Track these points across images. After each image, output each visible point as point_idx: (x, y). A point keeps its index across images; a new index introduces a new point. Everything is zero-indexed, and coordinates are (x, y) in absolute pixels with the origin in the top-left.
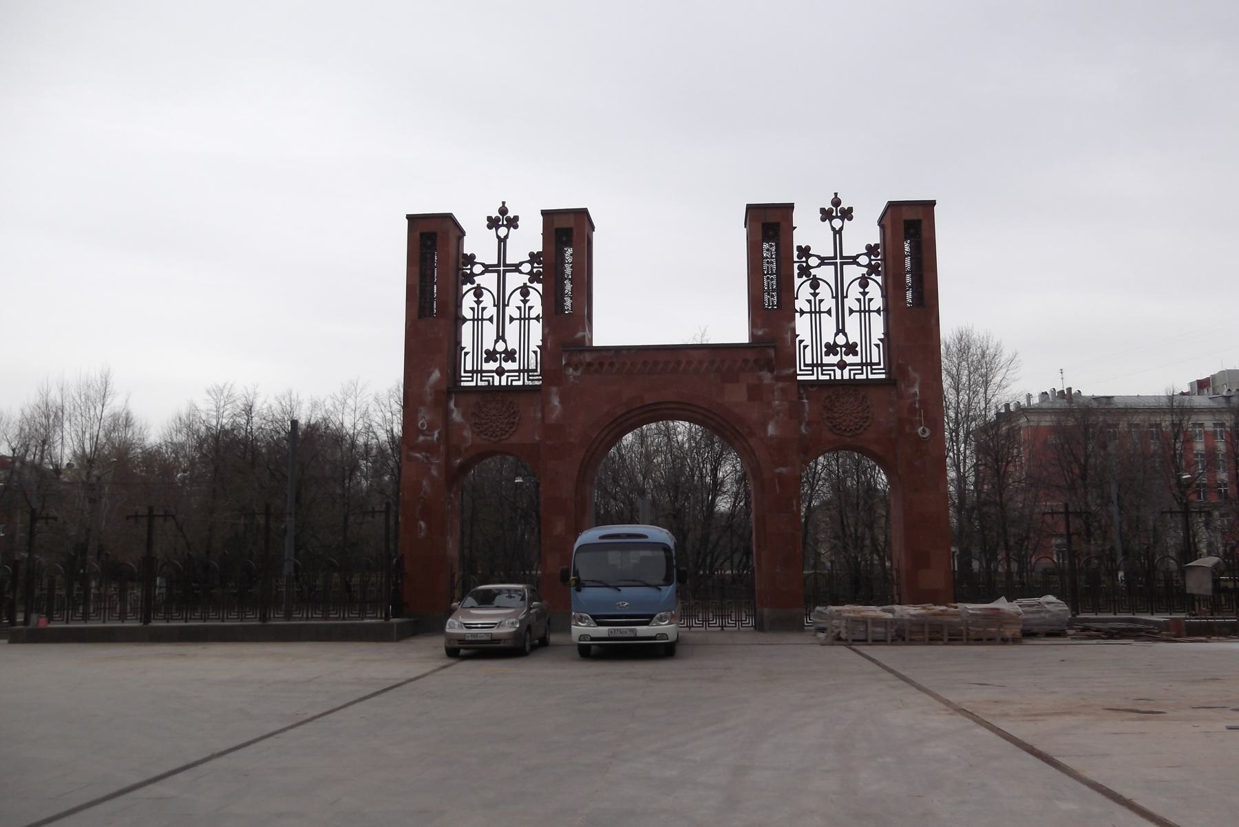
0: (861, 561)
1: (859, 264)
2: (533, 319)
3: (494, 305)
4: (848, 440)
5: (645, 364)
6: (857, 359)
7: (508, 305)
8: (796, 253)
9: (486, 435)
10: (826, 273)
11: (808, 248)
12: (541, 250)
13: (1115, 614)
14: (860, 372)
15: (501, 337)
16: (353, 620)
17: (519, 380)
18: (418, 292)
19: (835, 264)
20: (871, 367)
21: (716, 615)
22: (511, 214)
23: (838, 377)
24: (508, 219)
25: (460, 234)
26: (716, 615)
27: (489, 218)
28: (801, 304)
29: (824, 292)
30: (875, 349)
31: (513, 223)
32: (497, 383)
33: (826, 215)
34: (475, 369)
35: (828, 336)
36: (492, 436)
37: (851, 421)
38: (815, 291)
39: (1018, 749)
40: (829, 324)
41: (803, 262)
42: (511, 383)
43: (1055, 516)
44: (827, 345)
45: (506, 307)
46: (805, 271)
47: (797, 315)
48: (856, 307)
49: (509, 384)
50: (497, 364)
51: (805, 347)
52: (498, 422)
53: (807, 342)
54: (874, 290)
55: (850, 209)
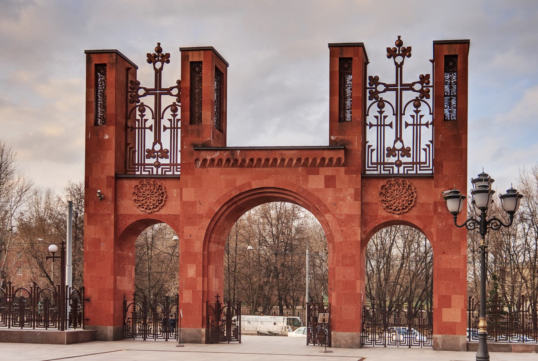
1: (414, 90)
2: (168, 128)
3: (394, 114)
4: (397, 216)
5: (323, 159)
6: (410, 160)
7: (404, 114)
8: (431, 94)
9: (143, 208)
10: (390, 96)
11: (377, 78)
12: (162, 88)
13: (47, 327)
14: (412, 168)
15: (399, 138)
16: (225, 84)
17: (377, 170)
19: (402, 85)
20: (384, 166)
21: (429, 338)
22: (405, 45)
23: (396, 171)
24: (163, 56)
25: (225, 66)
26: (429, 338)
27: (389, 50)
28: (371, 119)
29: (388, 110)
30: (423, 153)
31: (407, 52)
32: (155, 173)
33: (391, 53)
34: (415, 161)
35: (389, 142)
36: (146, 209)
37: (154, 200)
38: (381, 110)
39: (525, 354)
40: (390, 134)
41: (373, 88)
42: (165, 173)
43: (128, 142)
45: (403, 116)
46: (374, 95)
47: (368, 127)
48: (168, 125)
49: (406, 173)
50: (396, 158)
51: (372, 150)
52: (402, 197)
53: (374, 147)
54: (425, 109)
55: (409, 49)
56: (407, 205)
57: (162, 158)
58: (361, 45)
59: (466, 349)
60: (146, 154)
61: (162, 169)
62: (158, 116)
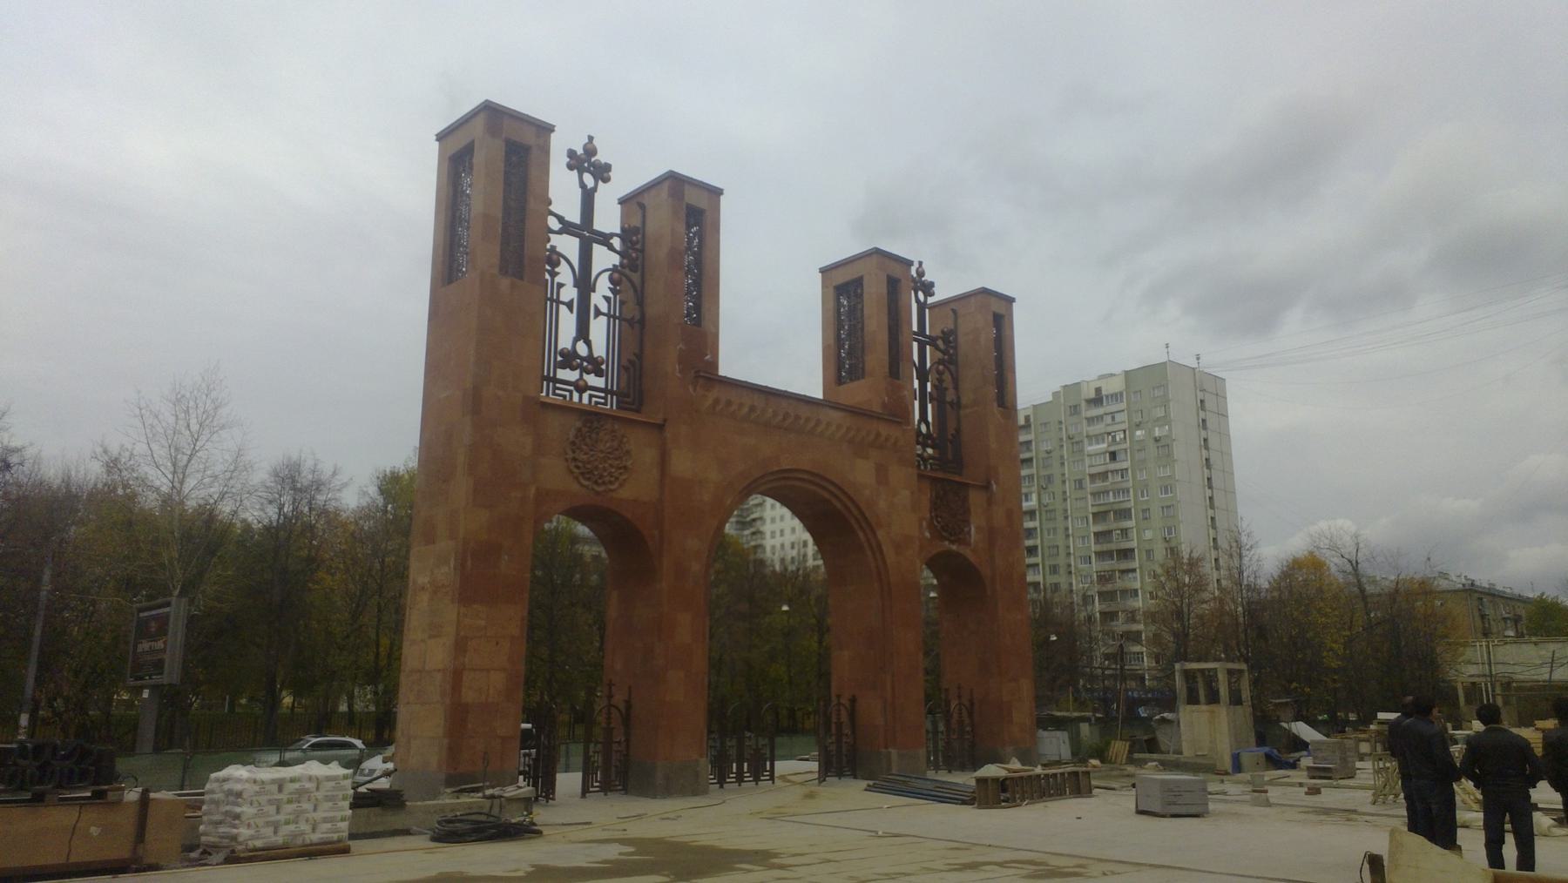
0: (17, 742)
17: (605, 404)
18: (1178, 489)
20: (554, 386)
44: (562, 353)
56: (607, 479)
57: (563, 367)
58: (1224, 380)
59: (354, 831)
60: (559, 358)
61: (591, 396)
62: (585, 283)
